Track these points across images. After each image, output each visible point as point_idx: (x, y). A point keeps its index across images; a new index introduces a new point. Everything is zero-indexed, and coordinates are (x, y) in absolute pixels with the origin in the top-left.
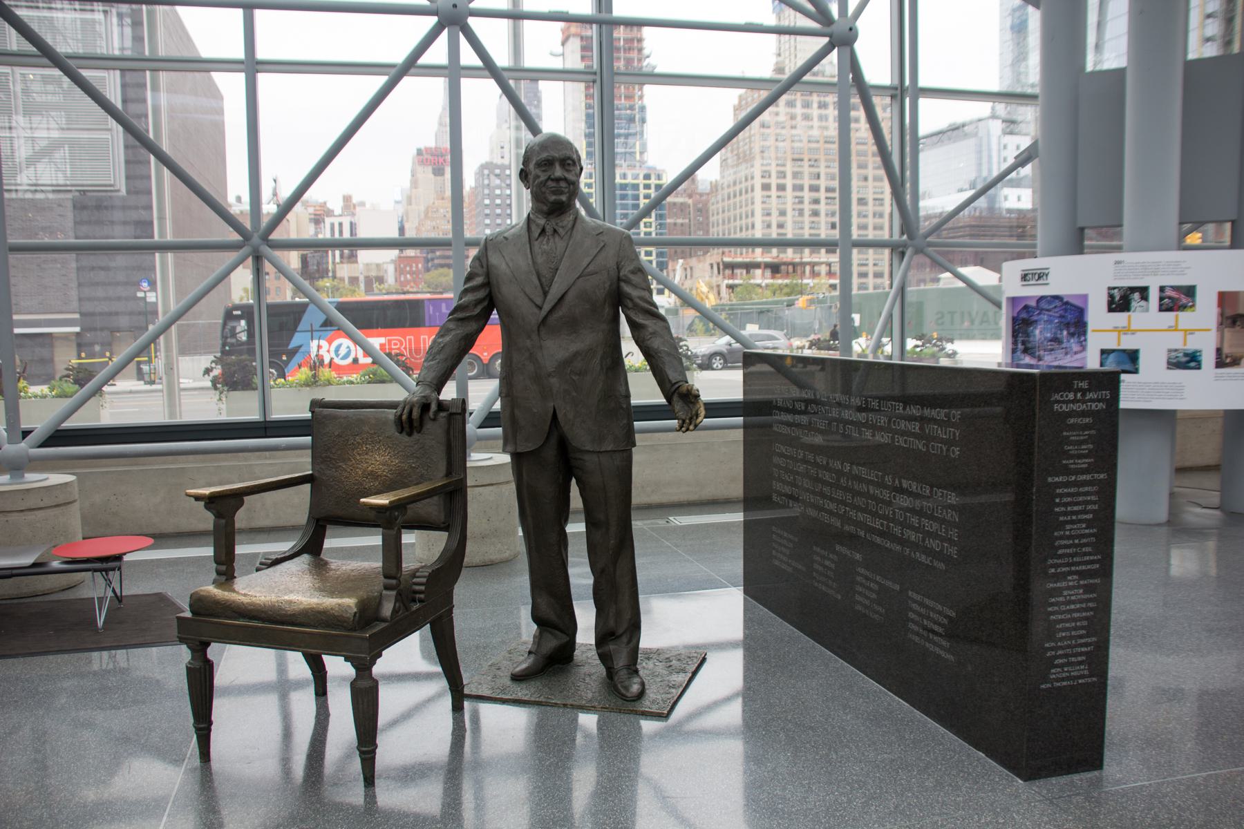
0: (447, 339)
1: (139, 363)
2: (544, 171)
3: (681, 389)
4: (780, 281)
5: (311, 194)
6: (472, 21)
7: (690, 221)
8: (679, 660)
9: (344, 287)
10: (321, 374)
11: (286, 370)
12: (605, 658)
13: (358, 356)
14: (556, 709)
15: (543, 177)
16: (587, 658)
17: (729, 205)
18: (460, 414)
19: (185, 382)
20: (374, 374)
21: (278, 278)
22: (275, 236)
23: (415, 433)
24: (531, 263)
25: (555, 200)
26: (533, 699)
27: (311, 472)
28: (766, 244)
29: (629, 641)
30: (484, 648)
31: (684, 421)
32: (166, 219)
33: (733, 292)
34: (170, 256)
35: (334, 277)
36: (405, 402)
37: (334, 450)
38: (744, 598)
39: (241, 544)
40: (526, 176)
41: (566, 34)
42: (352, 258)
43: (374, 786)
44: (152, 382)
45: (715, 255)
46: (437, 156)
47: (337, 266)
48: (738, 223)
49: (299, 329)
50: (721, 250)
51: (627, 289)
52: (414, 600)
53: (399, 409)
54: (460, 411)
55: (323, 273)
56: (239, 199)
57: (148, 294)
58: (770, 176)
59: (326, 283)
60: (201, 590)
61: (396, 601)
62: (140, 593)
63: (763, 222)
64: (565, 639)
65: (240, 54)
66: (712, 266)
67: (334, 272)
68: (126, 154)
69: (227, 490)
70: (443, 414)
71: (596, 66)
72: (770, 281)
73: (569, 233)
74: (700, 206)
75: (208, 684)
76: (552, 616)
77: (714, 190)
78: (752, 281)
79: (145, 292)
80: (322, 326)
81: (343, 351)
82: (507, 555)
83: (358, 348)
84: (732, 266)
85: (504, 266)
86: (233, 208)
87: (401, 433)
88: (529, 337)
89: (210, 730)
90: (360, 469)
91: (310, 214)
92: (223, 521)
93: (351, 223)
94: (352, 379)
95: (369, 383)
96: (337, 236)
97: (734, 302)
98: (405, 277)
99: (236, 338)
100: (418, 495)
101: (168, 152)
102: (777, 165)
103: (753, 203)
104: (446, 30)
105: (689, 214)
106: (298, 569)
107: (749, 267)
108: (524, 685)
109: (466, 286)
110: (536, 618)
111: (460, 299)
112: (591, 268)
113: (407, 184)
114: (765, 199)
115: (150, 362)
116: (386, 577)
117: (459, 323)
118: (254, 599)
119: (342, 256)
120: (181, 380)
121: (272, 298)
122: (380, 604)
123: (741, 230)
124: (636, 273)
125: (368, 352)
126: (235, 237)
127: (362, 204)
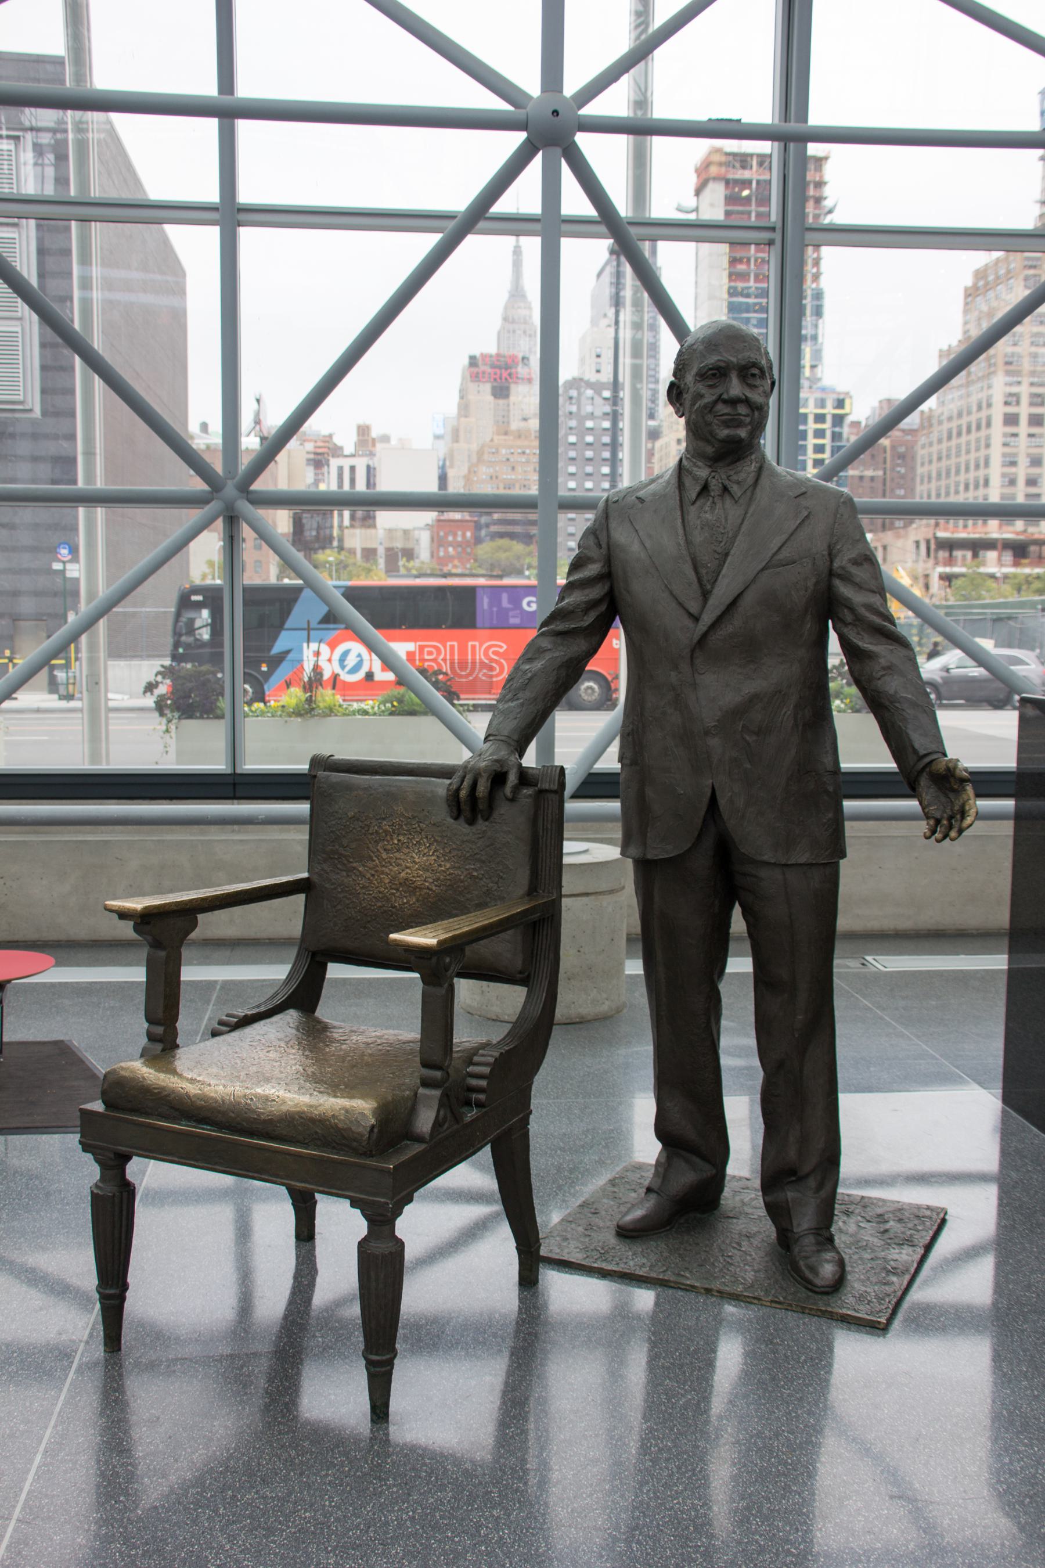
0: (538, 665)
1: (53, 668)
2: (711, 387)
3: (934, 767)
4: (1027, 570)
5: (315, 424)
6: (583, 140)
7: (885, 474)
8: (900, 1220)
9: (355, 564)
10: (319, 698)
11: (266, 687)
12: (777, 1211)
13: (374, 670)
14: (692, 1295)
15: (709, 398)
16: (744, 1204)
17: (949, 449)
18: (555, 792)
19: (116, 698)
20: (400, 701)
21: (258, 548)
22: (257, 486)
23: (480, 821)
24: (682, 542)
25: (728, 436)
26: (654, 1275)
27: (305, 875)
28: (1005, 513)
29: (820, 1187)
30: (571, 1171)
31: (938, 822)
32: (94, 454)
33: (950, 586)
34: (100, 512)
35: (341, 548)
36: (465, 767)
37: (345, 842)
38: (1004, 1112)
39: (190, 964)
40: (680, 394)
41: (704, 176)
42: (368, 521)
43: (387, 1421)
44: (70, 697)
45: (921, 529)
46: (500, 368)
47: (346, 531)
48: (962, 478)
49: (287, 625)
50: (932, 522)
51: (845, 590)
52: (468, 1103)
53: (456, 780)
54: (556, 787)
55: (324, 541)
56: (204, 427)
57: (69, 566)
58: (1018, 403)
59: (329, 556)
60: (122, 1068)
61: (441, 1105)
62: (31, 1039)
63: (1003, 475)
64: (708, 1171)
65: (212, 195)
66: (917, 543)
67: (341, 540)
68: (42, 356)
69: (170, 904)
70: (527, 791)
71: (774, 217)
72: (1010, 570)
73: (749, 493)
74: (902, 450)
75: (124, 1223)
76: (690, 1133)
77: (926, 424)
78: (982, 570)
79: (64, 563)
80: (322, 622)
81: (351, 661)
82: (605, 1008)
83: (374, 657)
84: (950, 546)
85: (636, 547)
86: (196, 441)
87: (456, 818)
88: (676, 667)
89: (123, 1299)
90: (387, 875)
91: (308, 453)
92: (163, 954)
93: (368, 467)
94: (366, 707)
95: (392, 714)
96: (346, 487)
97: (952, 602)
98: (446, 551)
99: (194, 635)
100: (484, 928)
101: (101, 352)
102: (1032, 384)
103: (988, 446)
104: (540, 154)
105: (885, 462)
106: (281, 1035)
107: (977, 547)
108: (638, 1248)
109: (571, 579)
110: (662, 1131)
111: (562, 599)
112: (785, 554)
113: (451, 406)
114: (1009, 439)
115: (67, 666)
116: (425, 1064)
117: (559, 640)
118: (207, 1089)
119: (353, 518)
120: (110, 696)
121: (251, 578)
122: (412, 1111)
123: (967, 487)
124: (861, 564)
125: (388, 664)
126: (199, 485)
127: (386, 439)
